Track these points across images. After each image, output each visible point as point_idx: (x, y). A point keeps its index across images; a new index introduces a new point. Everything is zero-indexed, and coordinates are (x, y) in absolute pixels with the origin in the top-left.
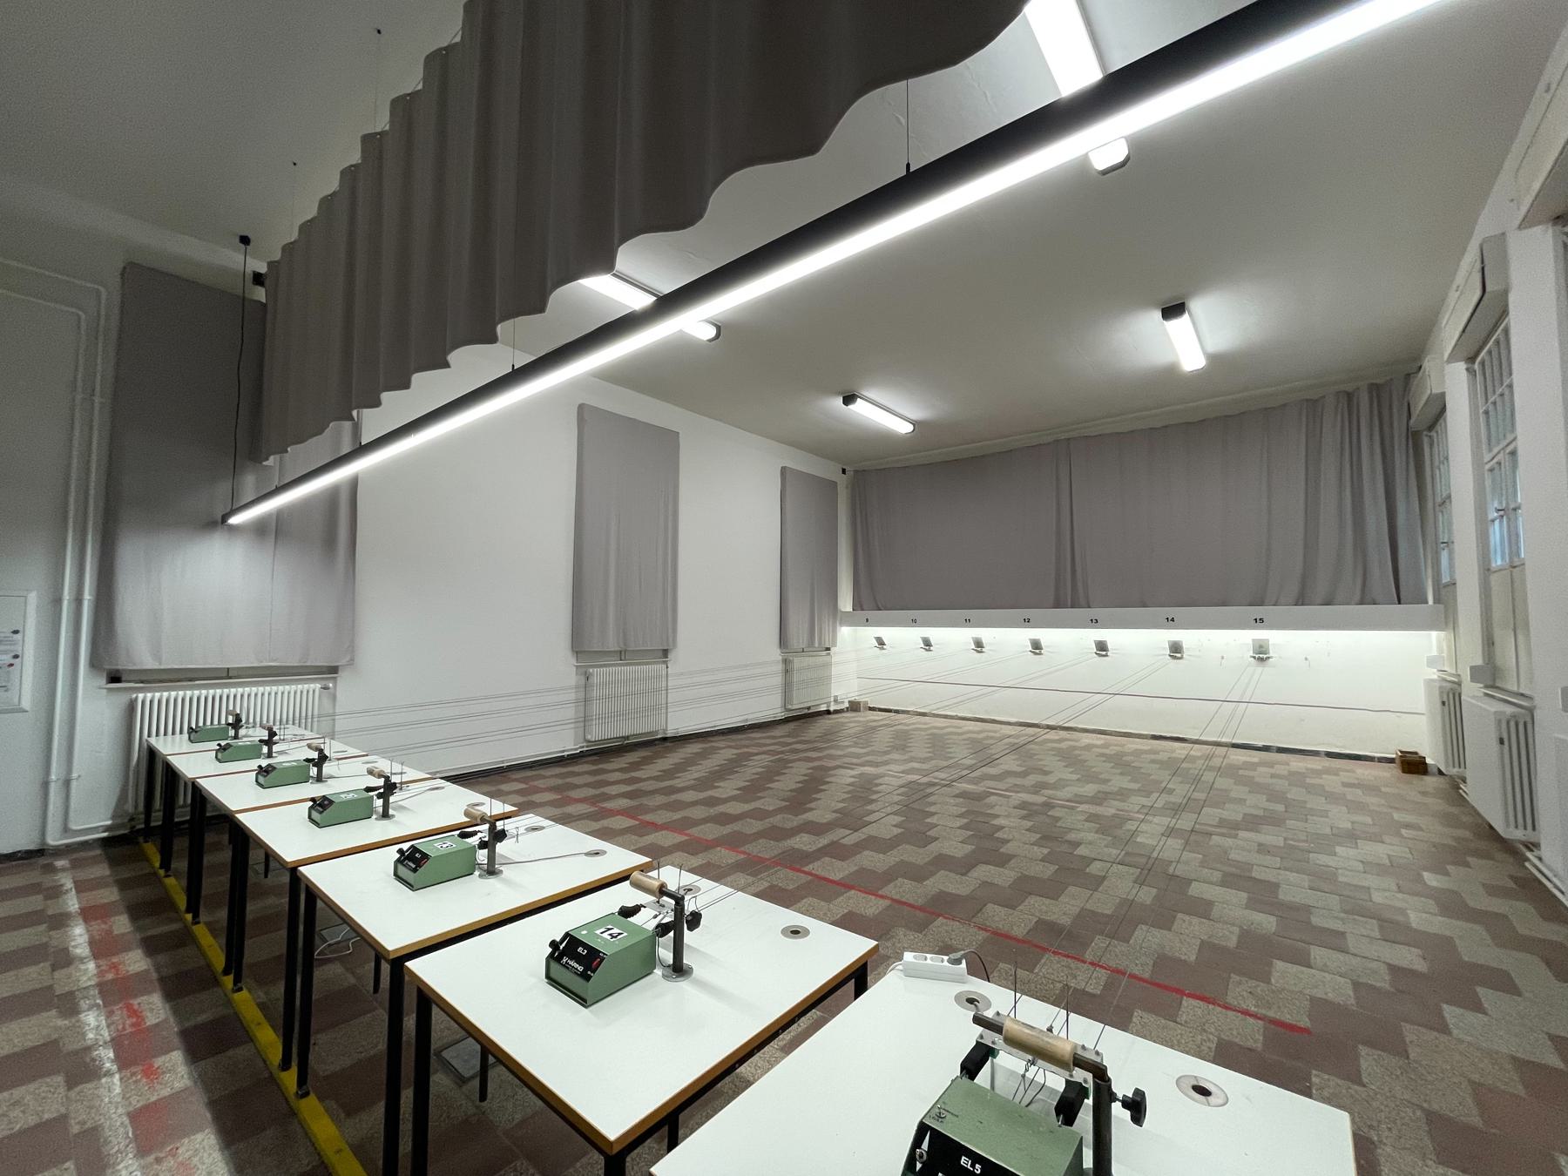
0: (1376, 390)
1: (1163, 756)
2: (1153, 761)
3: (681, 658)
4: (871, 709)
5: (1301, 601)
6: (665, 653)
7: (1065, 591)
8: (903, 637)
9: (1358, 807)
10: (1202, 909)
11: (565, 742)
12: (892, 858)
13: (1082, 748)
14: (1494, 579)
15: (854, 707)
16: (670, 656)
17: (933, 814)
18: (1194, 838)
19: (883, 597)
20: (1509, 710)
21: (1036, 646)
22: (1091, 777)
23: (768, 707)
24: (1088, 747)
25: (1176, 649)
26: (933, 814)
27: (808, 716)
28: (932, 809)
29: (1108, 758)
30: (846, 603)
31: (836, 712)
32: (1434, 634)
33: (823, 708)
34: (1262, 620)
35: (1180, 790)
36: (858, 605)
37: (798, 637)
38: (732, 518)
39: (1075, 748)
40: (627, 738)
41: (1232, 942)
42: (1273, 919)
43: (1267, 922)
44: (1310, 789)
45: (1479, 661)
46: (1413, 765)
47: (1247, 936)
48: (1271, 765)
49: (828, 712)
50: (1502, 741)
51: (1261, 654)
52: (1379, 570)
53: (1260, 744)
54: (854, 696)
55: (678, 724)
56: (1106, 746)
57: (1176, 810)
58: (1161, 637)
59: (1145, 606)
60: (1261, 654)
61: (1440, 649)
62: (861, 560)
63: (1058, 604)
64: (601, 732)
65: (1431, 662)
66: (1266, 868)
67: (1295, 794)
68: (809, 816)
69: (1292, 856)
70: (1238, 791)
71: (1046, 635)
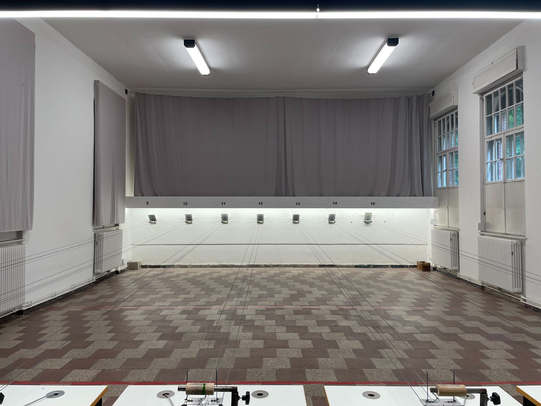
1: (215, 275)
2: (210, 279)
3: (32, 238)
4: (143, 267)
6: (19, 235)
7: (283, 186)
8: (170, 215)
10: (285, 344)
12: (65, 360)
13: (225, 276)
15: (132, 266)
16: (25, 236)
18: (268, 313)
19: (161, 183)
20: (515, 241)
23: (86, 277)
24: (178, 276)
25: (189, 218)
27: (106, 279)
30: (129, 192)
31: (122, 271)
32: (432, 210)
33: (114, 270)
34: (336, 203)
35: (256, 292)
36: (139, 191)
41: (301, 356)
42: (310, 342)
43: (309, 344)
44: (276, 282)
46: (426, 267)
48: (284, 273)
49: (117, 272)
50: (512, 254)
53: (366, 264)
55: (33, 298)
56: (186, 274)
58: (181, 212)
59: (321, 195)
60: (368, 220)
61: (435, 216)
63: (278, 194)
67: (270, 285)
68: (45, 347)
69: (307, 312)
70: (278, 287)
71: (266, 212)
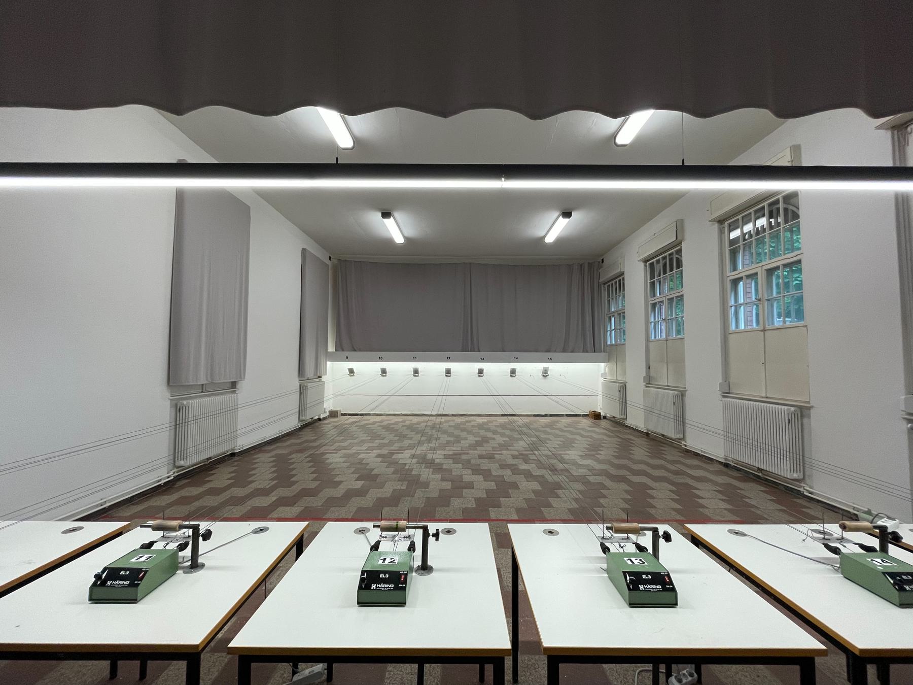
0: (590, 265)
4: (343, 415)
5: (564, 351)
6: (234, 385)
8: (367, 368)
9: (503, 435)
11: (163, 474)
14: (651, 345)
15: (333, 414)
17: (295, 475)
18: (455, 458)
21: (384, 372)
22: (379, 437)
23: (292, 423)
26: (295, 475)
27: (311, 425)
28: (293, 473)
29: (384, 427)
30: (331, 348)
31: (324, 419)
32: (602, 365)
36: (340, 347)
37: (309, 371)
38: (276, 283)
39: (367, 424)
40: (210, 458)
45: (644, 375)
47: (488, 491)
49: (319, 419)
51: (545, 373)
52: (584, 340)
54: (332, 408)
55: (244, 442)
57: (380, 447)
60: (545, 373)
62: (342, 320)
64: (192, 460)
65: (603, 375)
66: (485, 464)
70: (464, 434)
